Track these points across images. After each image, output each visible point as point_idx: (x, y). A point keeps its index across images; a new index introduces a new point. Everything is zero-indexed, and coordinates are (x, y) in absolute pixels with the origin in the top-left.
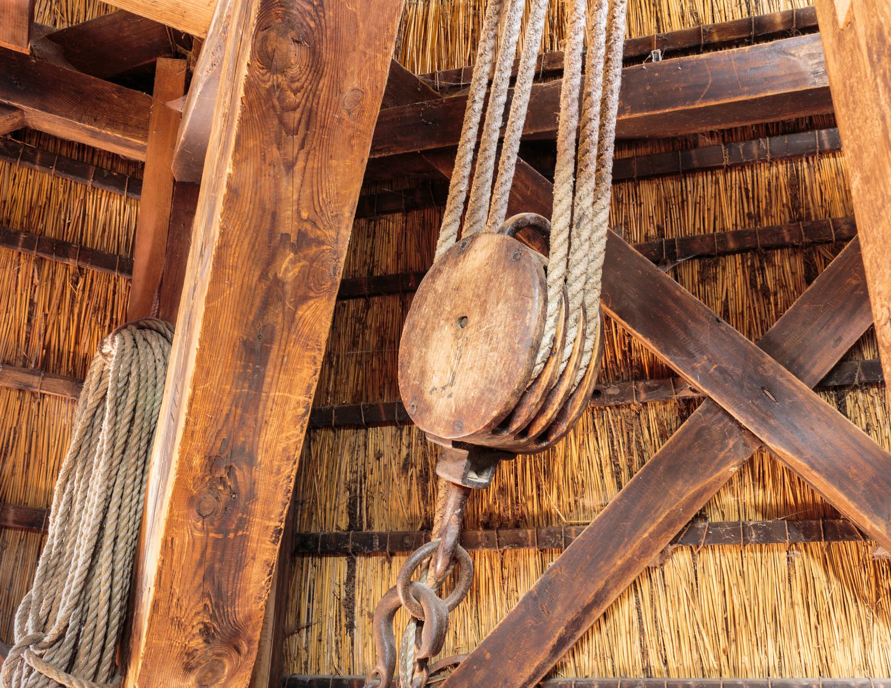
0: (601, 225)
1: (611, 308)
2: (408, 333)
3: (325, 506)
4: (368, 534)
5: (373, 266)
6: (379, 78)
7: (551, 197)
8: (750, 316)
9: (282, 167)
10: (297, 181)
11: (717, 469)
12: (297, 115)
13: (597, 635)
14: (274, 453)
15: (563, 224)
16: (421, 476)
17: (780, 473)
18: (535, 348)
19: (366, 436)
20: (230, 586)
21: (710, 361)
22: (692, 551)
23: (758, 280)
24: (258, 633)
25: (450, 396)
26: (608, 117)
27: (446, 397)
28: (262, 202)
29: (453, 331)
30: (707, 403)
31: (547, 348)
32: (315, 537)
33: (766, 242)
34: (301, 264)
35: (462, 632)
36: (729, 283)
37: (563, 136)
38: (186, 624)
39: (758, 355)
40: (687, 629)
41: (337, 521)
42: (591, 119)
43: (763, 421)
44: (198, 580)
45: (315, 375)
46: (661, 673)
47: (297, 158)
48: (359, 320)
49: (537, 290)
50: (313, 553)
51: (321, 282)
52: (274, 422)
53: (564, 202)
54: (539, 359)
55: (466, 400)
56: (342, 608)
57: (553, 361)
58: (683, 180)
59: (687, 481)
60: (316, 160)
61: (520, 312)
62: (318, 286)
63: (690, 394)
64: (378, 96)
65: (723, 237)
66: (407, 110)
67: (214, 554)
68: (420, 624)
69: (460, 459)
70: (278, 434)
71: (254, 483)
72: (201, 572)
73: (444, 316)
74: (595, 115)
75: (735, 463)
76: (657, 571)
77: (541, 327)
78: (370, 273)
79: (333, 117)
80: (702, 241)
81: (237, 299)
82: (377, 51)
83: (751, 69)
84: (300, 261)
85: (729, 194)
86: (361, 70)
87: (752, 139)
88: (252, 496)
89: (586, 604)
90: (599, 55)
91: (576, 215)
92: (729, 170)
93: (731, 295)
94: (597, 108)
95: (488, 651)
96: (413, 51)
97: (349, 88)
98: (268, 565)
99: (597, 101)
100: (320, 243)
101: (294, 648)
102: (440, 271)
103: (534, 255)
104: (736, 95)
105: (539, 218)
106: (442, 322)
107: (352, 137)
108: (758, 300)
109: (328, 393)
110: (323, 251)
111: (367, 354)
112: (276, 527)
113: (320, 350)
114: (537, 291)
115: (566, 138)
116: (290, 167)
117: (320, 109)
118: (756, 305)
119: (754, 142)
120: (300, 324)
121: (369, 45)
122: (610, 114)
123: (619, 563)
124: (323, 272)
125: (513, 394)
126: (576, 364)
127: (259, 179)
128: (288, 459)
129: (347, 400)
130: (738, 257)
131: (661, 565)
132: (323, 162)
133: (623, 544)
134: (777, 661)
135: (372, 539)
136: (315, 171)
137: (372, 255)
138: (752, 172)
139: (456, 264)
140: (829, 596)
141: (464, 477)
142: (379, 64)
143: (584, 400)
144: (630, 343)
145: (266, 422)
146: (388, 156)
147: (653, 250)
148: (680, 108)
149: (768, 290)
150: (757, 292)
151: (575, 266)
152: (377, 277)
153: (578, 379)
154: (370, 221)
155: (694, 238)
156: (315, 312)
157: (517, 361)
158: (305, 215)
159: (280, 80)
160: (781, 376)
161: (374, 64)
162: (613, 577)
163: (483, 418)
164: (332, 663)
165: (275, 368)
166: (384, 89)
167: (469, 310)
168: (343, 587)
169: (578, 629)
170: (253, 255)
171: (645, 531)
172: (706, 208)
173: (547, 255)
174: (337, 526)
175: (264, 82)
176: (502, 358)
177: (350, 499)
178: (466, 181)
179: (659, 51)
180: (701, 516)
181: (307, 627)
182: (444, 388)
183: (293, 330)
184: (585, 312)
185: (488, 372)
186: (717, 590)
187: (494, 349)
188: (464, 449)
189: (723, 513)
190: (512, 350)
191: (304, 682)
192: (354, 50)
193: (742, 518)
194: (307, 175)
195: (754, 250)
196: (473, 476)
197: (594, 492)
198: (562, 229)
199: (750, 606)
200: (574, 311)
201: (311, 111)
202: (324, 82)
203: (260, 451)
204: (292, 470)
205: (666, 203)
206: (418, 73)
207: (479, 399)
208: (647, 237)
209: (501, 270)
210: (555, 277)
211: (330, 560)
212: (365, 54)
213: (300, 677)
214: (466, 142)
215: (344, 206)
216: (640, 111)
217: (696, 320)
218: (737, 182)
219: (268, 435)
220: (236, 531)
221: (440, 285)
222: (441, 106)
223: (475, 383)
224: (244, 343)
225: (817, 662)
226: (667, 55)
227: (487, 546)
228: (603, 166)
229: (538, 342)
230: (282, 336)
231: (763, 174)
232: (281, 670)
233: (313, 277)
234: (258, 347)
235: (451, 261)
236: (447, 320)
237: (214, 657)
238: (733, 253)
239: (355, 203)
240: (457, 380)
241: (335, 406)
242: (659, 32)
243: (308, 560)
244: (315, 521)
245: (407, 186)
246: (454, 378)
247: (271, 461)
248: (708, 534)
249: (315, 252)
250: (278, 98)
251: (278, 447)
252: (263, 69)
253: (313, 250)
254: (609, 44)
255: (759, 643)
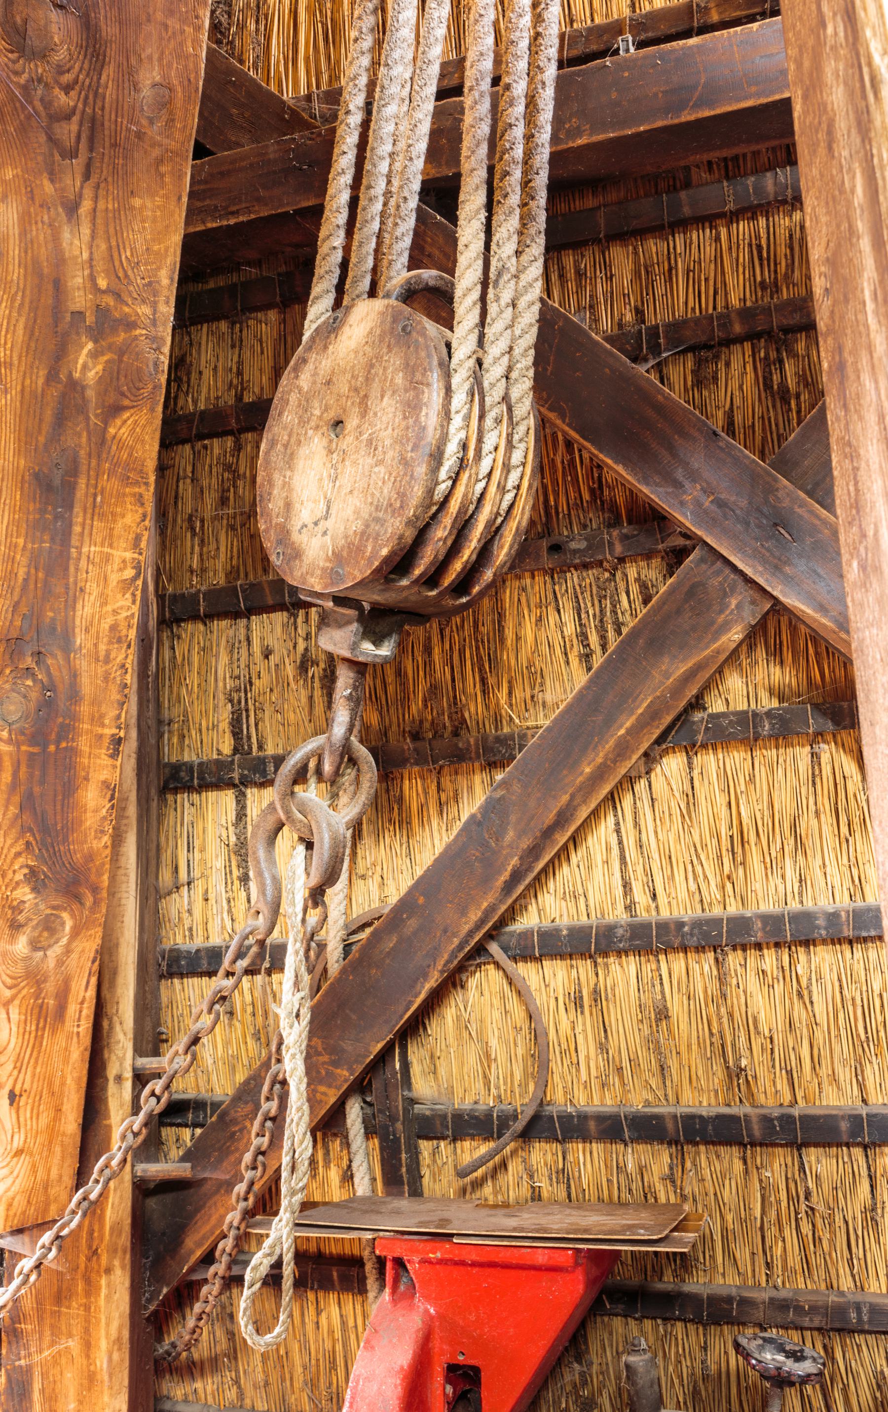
0: (531, 285)
1: (569, 425)
2: (267, 453)
3: (200, 724)
4: (259, 758)
5: (243, 389)
6: (191, 66)
7: (455, 241)
8: (764, 430)
9: (60, 210)
10: (86, 231)
11: (715, 639)
12: (74, 127)
13: (565, 869)
14: (98, 633)
15: (471, 280)
16: (326, 676)
17: (802, 643)
18: (437, 457)
19: (248, 628)
20: (59, 817)
21: (705, 492)
22: (687, 753)
23: (775, 377)
24: (106, 877)
25: (325, 533)
26: (539, 124)
27: (319, 535)
28: (36, 262)
29: (325, 442)
30: (702, 549)
31: (455, 458)
32: (190, 767)
33: (785, 322)
34: (105, 358)
35: (391, 876)
36: (734, 384)
37: (469, 148)
38: (5, 868)
39: (768, 479)
40: (680, 853)
41: (218, 743)
42: (510, 125)
43: (776, 568)
44: (13, 810)
45: (144, 520)
46: (648, 910)
47: (81, 196)
48: (228, 467)
49: (435, 375)
50: (189, 788)
51: (137, 385)
52: (93, 589)
53: (472, 247)
54: (443, 474)
55: (346, 537)
56: (233, 857)
57: (464, 477)
58: (670, 238)
59: (675, 657)
60: (110, 198)
61: (413, 407)
62: (134, 390)
63: (681, 542)
64: (193, 95)
65: (725, 319)
66: (271, 149)
67: (31, 776)
68: (309, 846)
69: (349, 623)
70: (101, 606)
71: (74, 676)
72: (16, 799)
73: (313, 424)
74: (517, 119)
75: (739, 628)
76: (642, 781)
77: (442, 426)
78: (239, 398)
79: (128, 130)
80: (696, 324)
81: (18, 412)
82: (184, 21)
83: (762, 57)
84: (103, 354)
85: (734, 255)
86: (162, 53)
87: (766, 170)
88: (74, 696)
89: (545, 826)
90: (521, 26)
91: (493, 269)
92: (734, 219)
93: (737, 402)
94: (520, 109)
95: (423, 894)
96: (278, 61)
97: (148, 82)
98: (108, 787)
99: (519, 97)
100: (131, 325)
101: (174, 913)
102: (305, 361)
103: (431, 328)
104: (739, 100)
105: (442, 278)
106: (310, 432)
107: (160, 161)
108: (774, 407)
109: (192, 572)
110: (136, 338)
111: (242, 514)
112: (113, 735)
113: (147, 484)
114: (435, 377)
115: (473, 152)
116: (72, 209)
117: (107, 117)
118: (772, 414)
119: (769, 174)
120: (114, 447)
121: (171, 13)
122: (541, 118)
123: (588, 770)
124: (139, 370)
125: (409, 523)
126: (499, 483)
127: (28, 228)
128: (119, 641)
129: (220, 580)
130: (747, 346)
131: (647, 773)
132: (121, 201)
133: (592, 746)
134: (796, 885)
135: (264, 763)
136: (111, 215)
137: (240, 373)
138: (767, 220)
139: (326, 347)
140: (864, 798)
141: (354, 647)
142: (189, 44)
143: (515, 535)
144: (600, 478)
145: (82, 590)
146: (249, 221)
147: (628, 343)
148: (659, 124)
149: (788, 391)
150: (773, 396)
151: (493, 342)
152: (249, 403)
153: (505, 505)
154: (233, 323)
155: (685, 322)
156: (134, 429)
157: (412, 476)
158: (102, 283)
159: (40, 71)
160: (800, 506)
161: (181, 44)
162: (580, 789)
163: (370, 560)
164: (223, 928)
165: (85, 512)
166: (201, 83)
167: (345, 410)
168: (231, 829)
169: (537, 858)
170: (33, 345)
171: (621, 727)
172: (703, 278)
173: (451, 329)
174: (218, 750)
175: (17, 73)
176: (390, 474)
177: (233, 713)
178: (342, 233)
179: (630, 39)
180: (697, 703)
181: (189, 884)
182: (316, 524)
183: (104, 456)
184: (510, 409)
185: (373, 494)
186: (721, 800)
187: (380, 463)
188: (350, 608)
189: (727, 700)
190: (404, 462)
191: (189, 952)
192: (149, 21)
193: (753, 706)
194: (99, 221)
195: (768, 334)
196: (367, 646)
197: (557, 683)
198: (470, 286)
199: (763, 819)
200: (492, 406)
201: (93, 120)
202: (109, 72)
203: (77, 630)
204: (126, 657)
205: (647, 272)
206: (288, 96)
207: (363, 533)
208: (620, 325)
209: (385, 350)
210: (462, 357)
211: (212, 796)
212: (166, 26)
213: (184, 948)
214: (339, 174)
215: (159, 268)
216: (604, 132)
217: (683, 434)
218: (747, 236)
219: (86, 610)
220: (58, 743)
221: (305, 380)
222: (319, 140)
223: (357, 512)
224: (36, 476)
225: (847, 883)
226: (640, 45)
227: (417, 763)
228: (533, 198)
229: (439, 448)
230: (89, 465)
231: (782, 222)
232: (158, 940)
233: (126, 376)
234: (57, 482)
235: (319, 344)
236: (317, 427)
237: (49, 911)
238: (739, 340)
239: (175, 263)
240: (333, 511)
241: (203, 588)
242: (634, 11)
243: (183, 798)
244: (189, 746)
245: (283, 269)
246: (328, 508)
247: (96, 645)
248: (707, 729)
249: (124, 339)
250: (42, 100)
251: (102, 625)
252: (12, 52)
253: (121, 337)
254: (539, 10)
255: (771, 866)
